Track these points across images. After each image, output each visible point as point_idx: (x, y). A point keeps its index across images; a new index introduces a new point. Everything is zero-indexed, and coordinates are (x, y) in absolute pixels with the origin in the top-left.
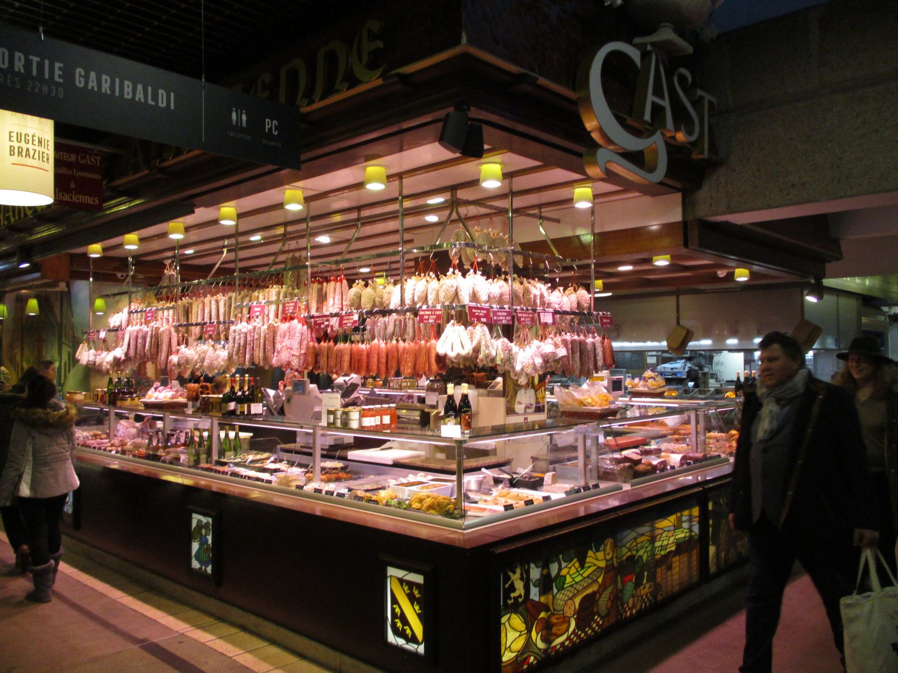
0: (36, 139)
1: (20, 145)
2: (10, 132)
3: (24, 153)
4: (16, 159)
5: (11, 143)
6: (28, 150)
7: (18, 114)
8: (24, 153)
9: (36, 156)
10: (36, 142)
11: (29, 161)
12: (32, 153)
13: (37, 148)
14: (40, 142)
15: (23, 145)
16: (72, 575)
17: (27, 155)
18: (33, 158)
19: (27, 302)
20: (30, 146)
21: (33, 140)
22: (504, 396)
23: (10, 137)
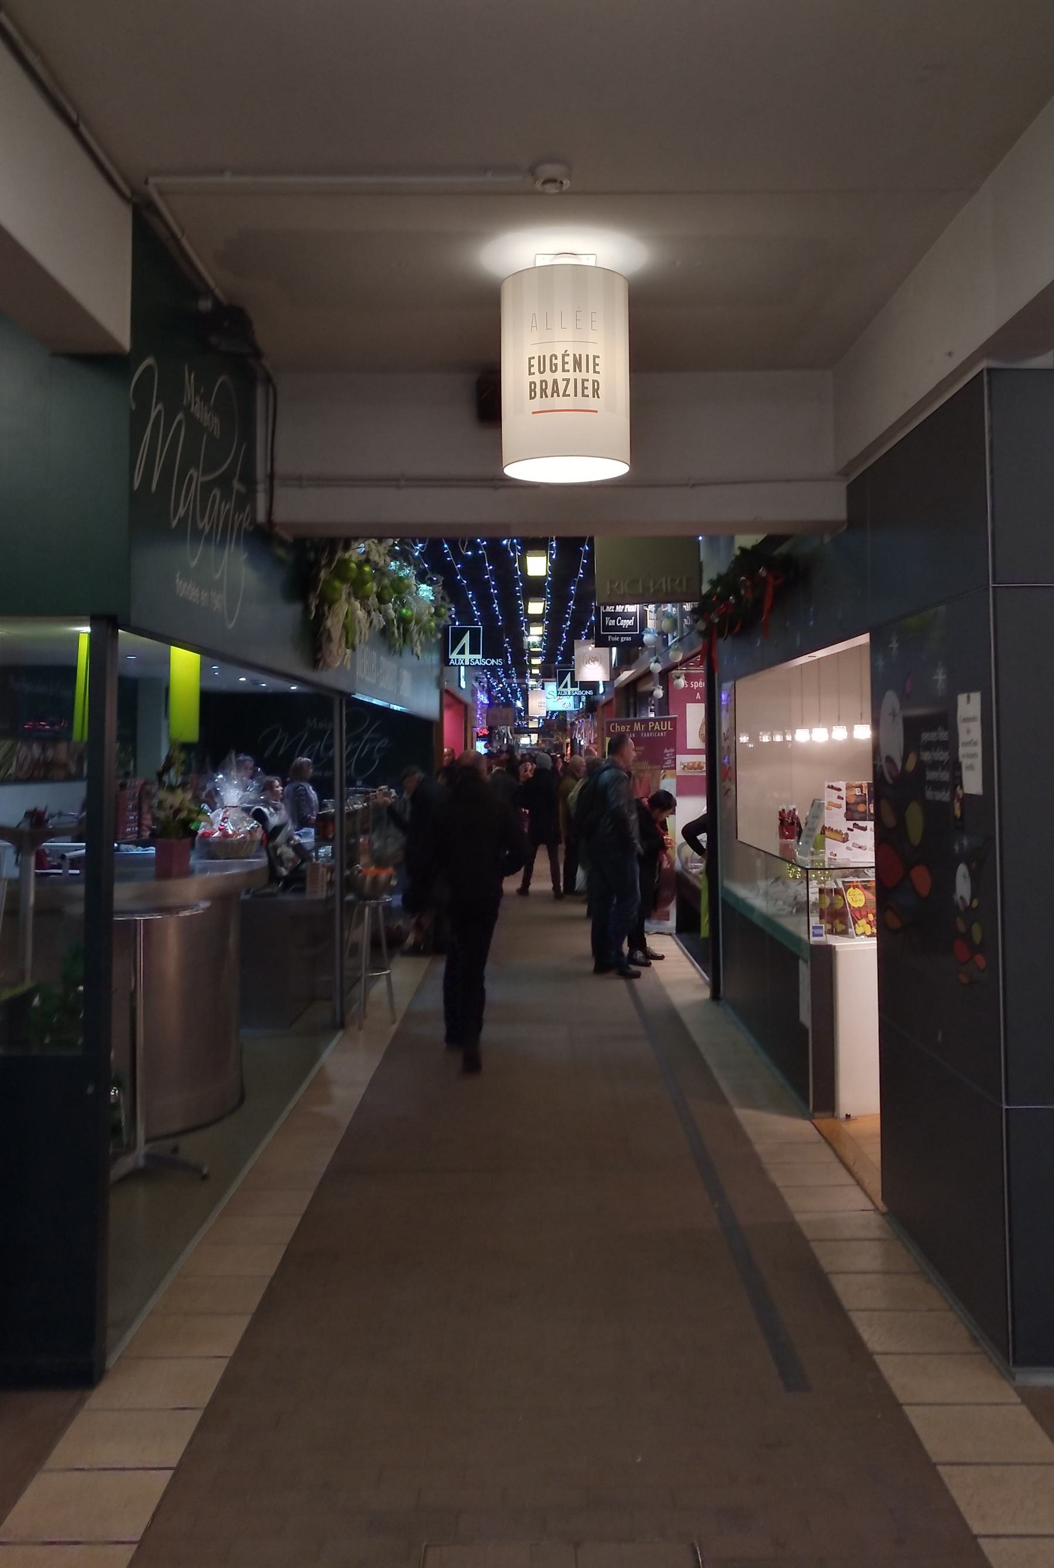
0: (570, 359)
1: (544, 377)
2: (530, 359)
3: (549, 391)
4: (538, 403)
5: (532, 378)
6: (555, 382)
7: (1008, 319)
8: (549, 391)
9: (570, 390)
10: (570, 366)
11: (559, 402)
12: (561, 386)
13: (571, 375)
14: (577, 363)
15: (549, 376)
16: (107, 724)
17: (555, 391)
18: (583, 395)
19: (923, 762)
20: (559, 375)
21: (564, 363)
22: (824, 829)
23: (531, 366)
